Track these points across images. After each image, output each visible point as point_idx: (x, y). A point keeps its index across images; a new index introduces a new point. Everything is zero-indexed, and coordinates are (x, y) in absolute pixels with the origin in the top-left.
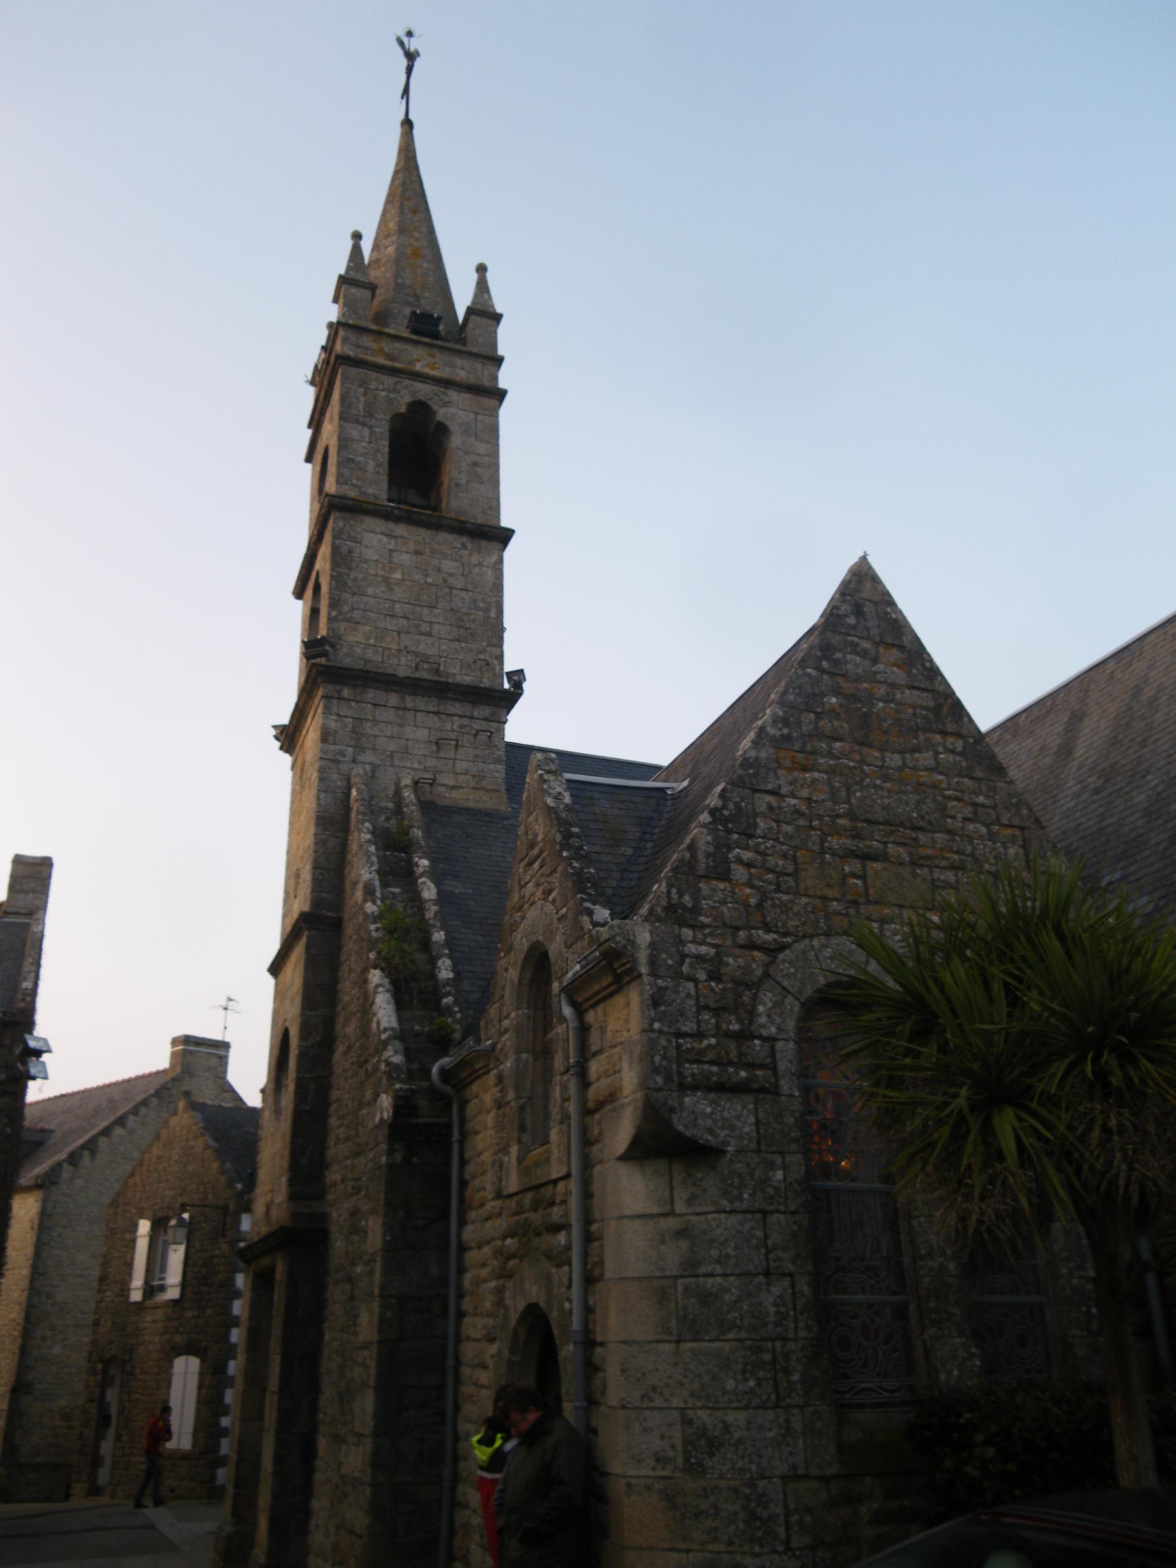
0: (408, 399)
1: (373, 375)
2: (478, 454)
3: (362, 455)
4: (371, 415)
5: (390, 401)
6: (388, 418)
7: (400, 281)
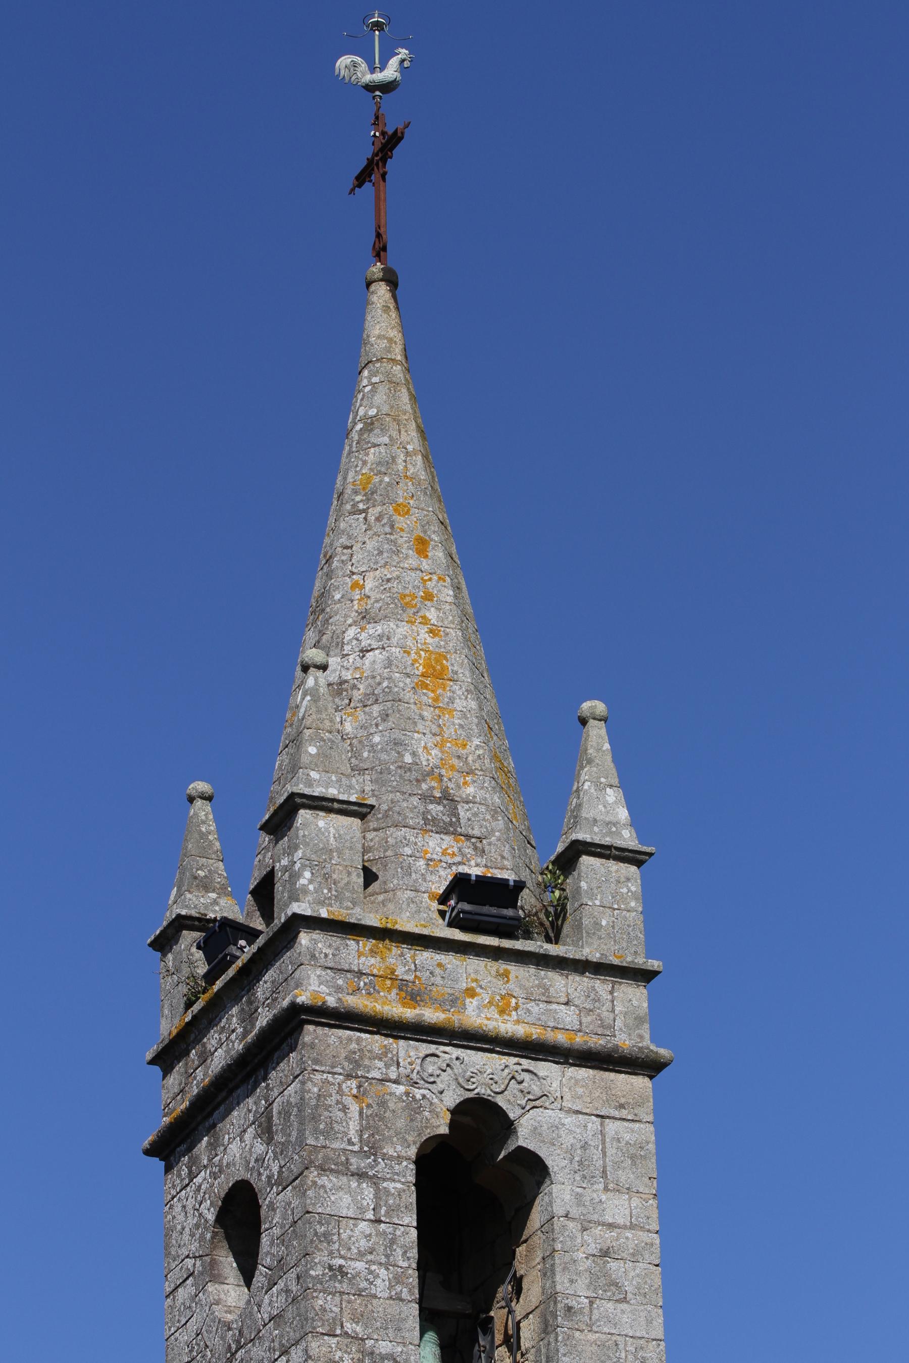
0: (452, 1098)
1: (376, 1042)
2: (611, 1226)
3: (361, 1254)
4: (373, 1150)
5: (414, 1108)
6: (412, 1152)
7: (408, 759)
